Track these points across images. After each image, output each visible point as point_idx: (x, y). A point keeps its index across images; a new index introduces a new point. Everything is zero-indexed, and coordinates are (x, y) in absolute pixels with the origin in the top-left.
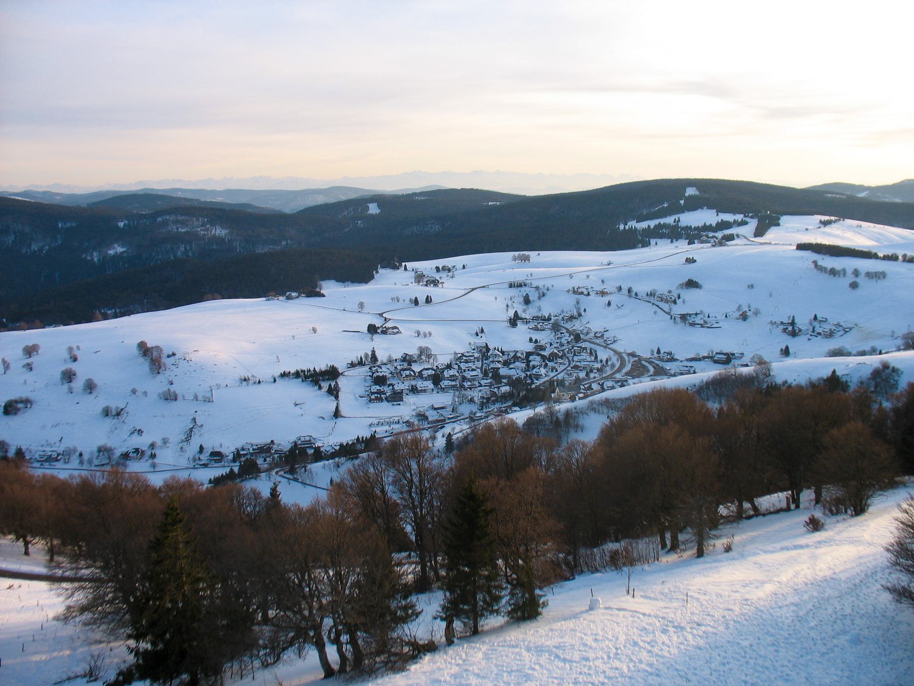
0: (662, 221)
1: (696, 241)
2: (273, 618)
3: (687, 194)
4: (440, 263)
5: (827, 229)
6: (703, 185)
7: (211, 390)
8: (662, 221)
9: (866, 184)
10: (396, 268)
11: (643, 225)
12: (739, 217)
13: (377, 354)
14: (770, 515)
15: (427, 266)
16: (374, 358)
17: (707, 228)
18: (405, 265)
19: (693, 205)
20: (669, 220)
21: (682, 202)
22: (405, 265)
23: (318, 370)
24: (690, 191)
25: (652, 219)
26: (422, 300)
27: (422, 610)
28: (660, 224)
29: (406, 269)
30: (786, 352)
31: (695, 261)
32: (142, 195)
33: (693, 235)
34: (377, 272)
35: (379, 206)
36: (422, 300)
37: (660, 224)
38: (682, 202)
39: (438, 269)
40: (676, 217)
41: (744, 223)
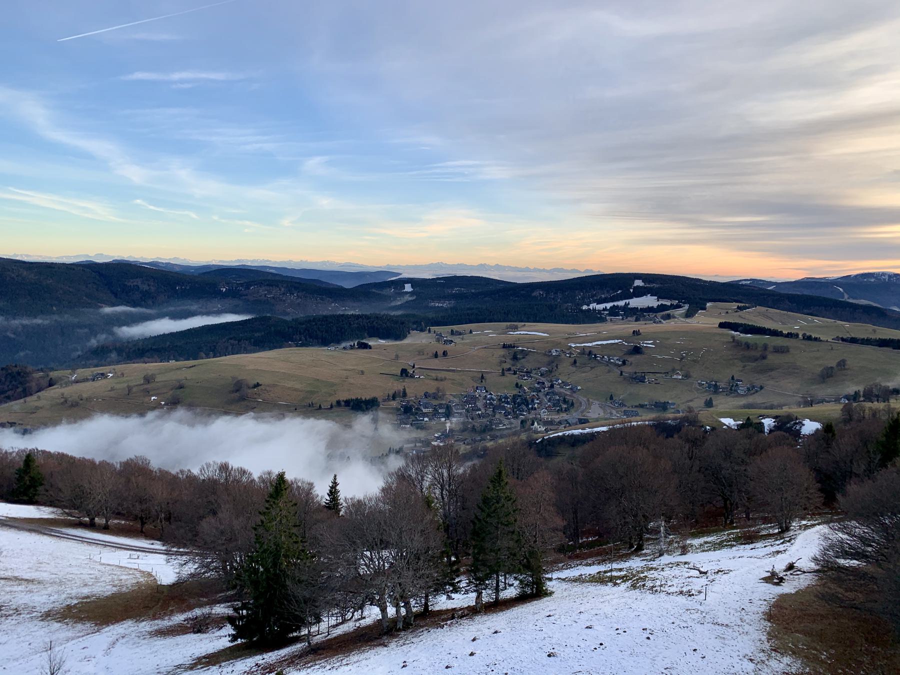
0: (616, 304)
1: (641, 319)
2: (407, 614)
3: (635, 285)
4: (455, 328)
5: (741, 313)
6: (648, 278)
7: (690, 594)
8: (616, 304)
9: (773, 280)
10: (422, 330)
11: (601, 307)
12: (675, 302)
13: (407, 391)
14: (162, 257)
15: (444, 330)
16: (405, 394)
17: (650, 310)
18: (430, 329)
19: (639, 293)
20: (621, 303)
21: (632, 290)
22: (430, 329)
23: (364, 399)
24: (638, 283)
25: (607, 302)
26: (440, 353)
27: (454, 599)
28: (614, 305)
29: (429, 331)
30: (709, 404)
31: (640, 334)
32: (374, 337)
33: (639, 314)
34: (409, 333)
35: (412, 287)
36: (440, 353)
37: (614, 305)
38: (632, 290)
39: (452, 333)
40: (627, 301)
41: (678, 307)
